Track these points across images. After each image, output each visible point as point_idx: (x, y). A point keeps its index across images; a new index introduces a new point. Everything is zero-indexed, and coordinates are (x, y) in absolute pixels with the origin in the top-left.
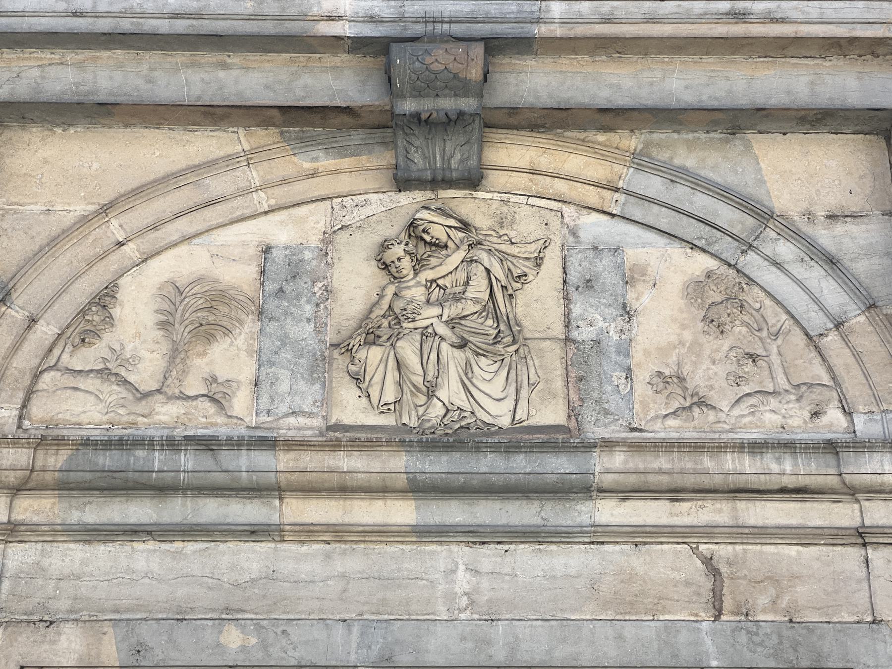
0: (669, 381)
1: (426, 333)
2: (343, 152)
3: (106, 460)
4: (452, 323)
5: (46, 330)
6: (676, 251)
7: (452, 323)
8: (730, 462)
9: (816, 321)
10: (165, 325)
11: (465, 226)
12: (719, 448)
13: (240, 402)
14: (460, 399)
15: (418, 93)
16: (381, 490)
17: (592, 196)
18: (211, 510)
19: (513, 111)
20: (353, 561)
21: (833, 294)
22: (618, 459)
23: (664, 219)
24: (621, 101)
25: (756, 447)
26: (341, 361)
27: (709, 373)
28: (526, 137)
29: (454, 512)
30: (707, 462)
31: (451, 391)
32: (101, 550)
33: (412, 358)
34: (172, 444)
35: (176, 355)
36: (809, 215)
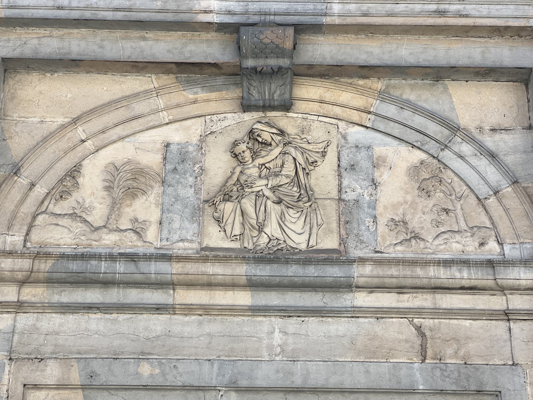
0: (398, 224)
1: (258, 195)
2: (212, 89)
3: (74, 266)
4: (274, 189)
5: (40, 190)
6: (404, 149)
7: (274, 189)
8: (432, 271)
9: (483, 190)
10: (108, 189)
11: (282, 133)
12: (426, 263)
13: (151, 234)
14: (278, 234)
15: (256, 56)
16: (231, 285)
17: (355, 116)
18: (134, 295)
19: (311, 66)
20: (214, 326)
21: (493, 174)
22: (368, 269)
23: (397, 130)
24: (373, 61)
25: (447, 263)
26: (209, 210)
27: (421, 220)
28: (318, 82)
29: (273, 299)
30: (419, 271)
31: (272, 229)
32: (71, 318)
33: (250, 209)
34: (112, 257)
35: (115, 206)
36: (480, 129)
